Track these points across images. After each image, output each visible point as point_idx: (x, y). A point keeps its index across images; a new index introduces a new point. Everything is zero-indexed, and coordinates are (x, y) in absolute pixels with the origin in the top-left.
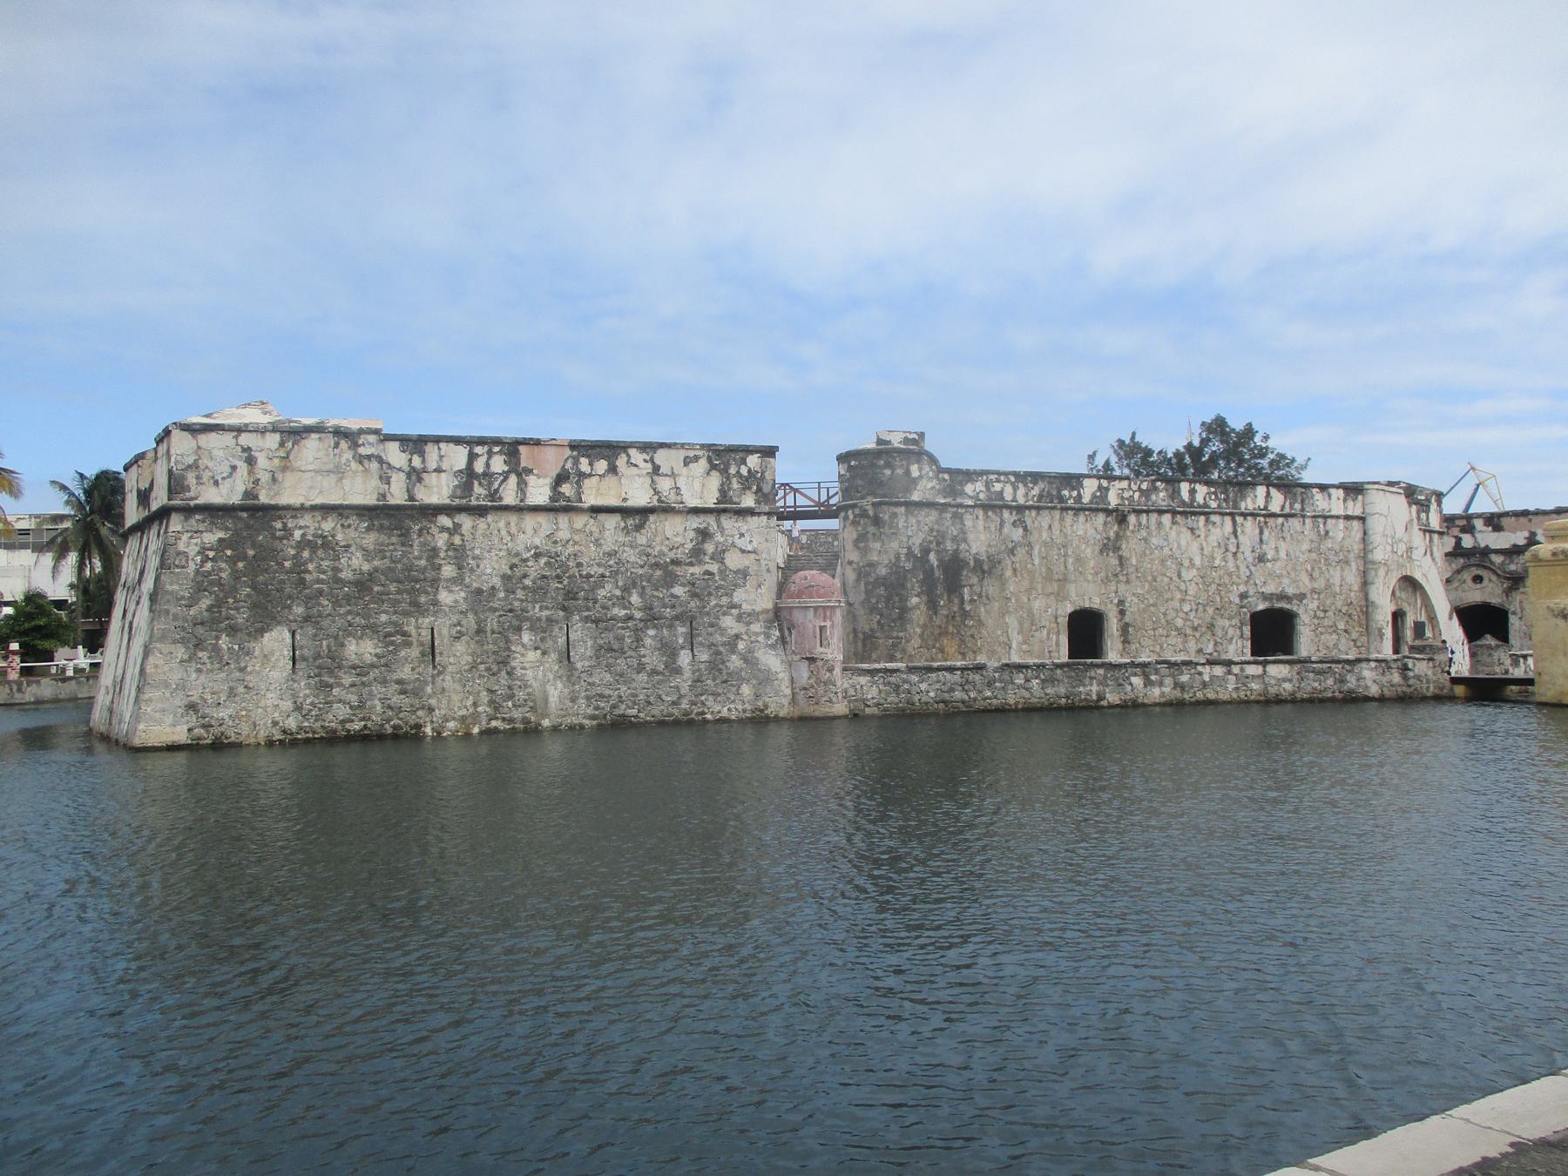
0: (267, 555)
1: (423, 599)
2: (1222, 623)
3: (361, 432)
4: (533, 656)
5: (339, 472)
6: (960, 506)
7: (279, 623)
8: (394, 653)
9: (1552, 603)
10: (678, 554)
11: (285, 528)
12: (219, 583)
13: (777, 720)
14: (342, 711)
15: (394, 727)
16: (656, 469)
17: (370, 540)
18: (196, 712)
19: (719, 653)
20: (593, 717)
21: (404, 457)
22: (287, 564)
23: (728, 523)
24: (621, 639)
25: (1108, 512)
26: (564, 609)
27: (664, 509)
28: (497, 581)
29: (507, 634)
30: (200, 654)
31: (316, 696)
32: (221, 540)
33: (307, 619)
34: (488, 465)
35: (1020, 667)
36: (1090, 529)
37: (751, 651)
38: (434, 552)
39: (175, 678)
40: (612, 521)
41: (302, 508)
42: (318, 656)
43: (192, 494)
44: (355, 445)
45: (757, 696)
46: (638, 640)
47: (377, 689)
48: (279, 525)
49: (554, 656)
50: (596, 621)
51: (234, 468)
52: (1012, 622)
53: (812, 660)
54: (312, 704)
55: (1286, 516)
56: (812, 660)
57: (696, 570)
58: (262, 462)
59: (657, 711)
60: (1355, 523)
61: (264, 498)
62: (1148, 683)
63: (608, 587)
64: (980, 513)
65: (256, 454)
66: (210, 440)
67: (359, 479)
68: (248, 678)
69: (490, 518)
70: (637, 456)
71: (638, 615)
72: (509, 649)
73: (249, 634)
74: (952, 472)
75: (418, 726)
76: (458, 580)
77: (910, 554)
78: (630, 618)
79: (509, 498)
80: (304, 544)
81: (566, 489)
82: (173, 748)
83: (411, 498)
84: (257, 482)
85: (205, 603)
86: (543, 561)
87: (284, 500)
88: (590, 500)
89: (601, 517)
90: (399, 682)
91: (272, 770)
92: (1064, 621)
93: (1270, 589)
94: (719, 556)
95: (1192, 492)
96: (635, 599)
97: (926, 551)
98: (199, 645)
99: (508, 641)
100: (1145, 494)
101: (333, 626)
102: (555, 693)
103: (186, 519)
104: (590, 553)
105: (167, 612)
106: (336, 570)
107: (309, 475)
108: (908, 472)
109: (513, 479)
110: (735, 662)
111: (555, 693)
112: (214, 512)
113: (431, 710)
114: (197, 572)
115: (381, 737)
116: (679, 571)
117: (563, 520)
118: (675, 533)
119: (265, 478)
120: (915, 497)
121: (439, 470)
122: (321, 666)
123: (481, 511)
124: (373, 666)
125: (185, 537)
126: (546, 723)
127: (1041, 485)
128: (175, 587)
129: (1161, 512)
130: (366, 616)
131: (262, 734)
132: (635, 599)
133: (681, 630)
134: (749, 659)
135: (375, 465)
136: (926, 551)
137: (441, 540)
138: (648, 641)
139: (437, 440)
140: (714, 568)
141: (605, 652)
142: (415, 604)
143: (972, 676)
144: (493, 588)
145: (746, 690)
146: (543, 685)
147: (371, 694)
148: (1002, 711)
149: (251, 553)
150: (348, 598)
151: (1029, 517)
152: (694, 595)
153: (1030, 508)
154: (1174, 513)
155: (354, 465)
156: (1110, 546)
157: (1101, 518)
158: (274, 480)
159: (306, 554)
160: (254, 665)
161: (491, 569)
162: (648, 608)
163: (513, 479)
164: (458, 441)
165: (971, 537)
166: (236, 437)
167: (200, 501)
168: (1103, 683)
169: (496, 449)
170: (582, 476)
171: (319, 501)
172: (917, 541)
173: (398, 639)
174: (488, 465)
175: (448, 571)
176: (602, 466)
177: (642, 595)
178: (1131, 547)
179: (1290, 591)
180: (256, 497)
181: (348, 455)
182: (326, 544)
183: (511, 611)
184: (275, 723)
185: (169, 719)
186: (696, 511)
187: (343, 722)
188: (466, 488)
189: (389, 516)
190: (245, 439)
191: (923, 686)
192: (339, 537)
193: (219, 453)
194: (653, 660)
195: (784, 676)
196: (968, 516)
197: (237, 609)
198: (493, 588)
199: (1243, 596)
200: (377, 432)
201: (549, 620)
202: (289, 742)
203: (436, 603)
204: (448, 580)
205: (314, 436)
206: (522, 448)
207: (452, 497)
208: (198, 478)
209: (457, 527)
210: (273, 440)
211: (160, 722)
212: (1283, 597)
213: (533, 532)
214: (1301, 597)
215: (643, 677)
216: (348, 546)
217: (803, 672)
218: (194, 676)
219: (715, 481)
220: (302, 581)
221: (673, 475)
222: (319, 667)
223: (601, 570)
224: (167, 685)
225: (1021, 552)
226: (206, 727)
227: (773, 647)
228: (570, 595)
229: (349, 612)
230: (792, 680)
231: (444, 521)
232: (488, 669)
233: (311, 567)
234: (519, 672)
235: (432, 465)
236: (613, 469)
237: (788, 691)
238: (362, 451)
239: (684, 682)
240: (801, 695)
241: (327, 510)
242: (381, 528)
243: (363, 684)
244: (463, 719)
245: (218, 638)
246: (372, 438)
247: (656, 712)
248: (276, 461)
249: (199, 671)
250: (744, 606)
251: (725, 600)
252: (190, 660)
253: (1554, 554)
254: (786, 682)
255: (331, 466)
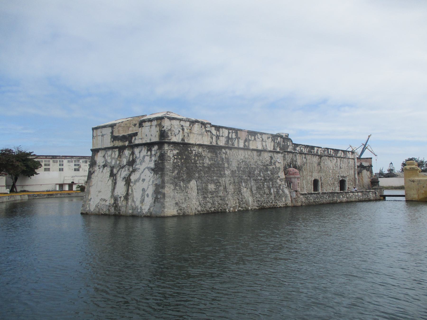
0: (188, 158)
1: (222, 173)
2: (335, 183)
3: (207, 123)
4: (245, 189)
5: (202, 134)
6: (296, 153)
7: (193, 179)
8: (218, 188)
9: (409, 179)
10: (268, 163)
11: (191, 150)
12: (178, 166)
13: (289, 207)
14: (209, 205)
15: (221, 210)
16: (263, 139)
17: (209, 155)
18: (178, 205)
19: (277, 189)
20: (258, 207)
21: (215, 131)
22: (193, 161)
23: (275, 155)
24: (260, 185)
25: (318, 155)
26: (249, 176)
27: (264, 150)
28: (236, 168)
29: (240, 183)
30: (177, 187)
31: (204, 201)
32: (177, 153)
33: (199, 178)
34: (232, 136)
35: (325, 193)
36: (315, 159)
37: (283, 189)
38: (223, 159)
39: (172, 195)
40: (255, 153)
41: (196, 145)
42: (203, 189)
43: (170, 138)
44: (205, 127)
45: (285, 201)
46: (264, 186)
47: (216, 198)
48: (190, 150)
49: (249, 189)
50: (255, 180)
51: (179, 131)
52: (304, 182)
53: (296, 191)
54: (203, 203)
55: (344, 158)
56: (296, 191)
57: (271, 167)
58: (186, 130)
59: (269, 204)
60: (353, 160)
61: (186, 141)
62: (343, 197)
63: (257, 171)
64: (299, 154)
65: (184, 128)
66: (175, 122)
67: (206, 137)
68: (188, 195)
69: (233, 150)
70: (259, 136)
71: (263, 179)
72: (240, 187)
73: (187, 182)
74: (295, 144)
75: (225, 209)
76: (228, 168)
77: (288, 164)
78: (261, 179)
79: (236, 146)
80: (196, 155)
81: (246, 144)
82: (174, 216)
83: (217, 144)
84: (184, 136)
85: (176, 172)
86: (244, 163)
87: (191, 142)
88: (251, 147)
89: (253, 152)
90: (220, 196)
91: (195, 223)
92: (312, 182)
93: (342, 175)
94: (275, 164)
95: (331, 151)
96: (262, 174)
97: (290, 164)
98: (176, 185)
99: (240, 185)
100: (324, 151)
101: (205, 180)
102: (250, 199)
103: (169, 146)
104: (252, 161)
105: (168, 174)
106: (203, 163)
107: (196, 135)
108: (287, 144)
109: (237, 140)
110: (281, 192)
111: (250, 199)
112: (174, 143)
113: (227, 205)
114: (173, 162)
115: (218, 212)
116: (269, 167)
117: (246, 152)
118: (266, 156)
119: (186, 135)
120: (289, 150)
121: (222, 136)
122: (203, 191)
123: (230, 148)
124: (214, 192)
125: (169, 151)
126: (250, 208)
127: (309, 148)
128: (169, 167)
129: (326, 156)
130: (211, 178)
131: (193, 212)
132: (262, 174)
133: (271, 183)
134: (283, 192)
135: (209, 134)
136: (290, 164)
137: (224, 156)
138: (265, 186)
139: (222, 127)
140: (274, 167)
141: (258, 188)
142: (221, 174)
143: (318, 196)
144: (235, 170)
145: (283, 199)
146: (248, 198)
147: (215, 200)
148: (323, 204)
149: (185, 157)
150: (207, 172)
151: (307, 155)
152: (272, 174)
153: (307, 154)
154: (328, 156)
155: (205, 133)
156: (319, 164)
157: (317, 157)
158: (188, 136)
159: (196, 158)
160: (189, 191)
161: (234, 165)
162: (264, 177)
163: (237, 140)
164: (226, 128)
165: (298, 160)
166: (180, 122)
167: (171, 141)
168: (337, 197)
169: (234, 131)
170: (250, 140)
171: (198, 143)
172: (289, 161)
173: (218, 184)
174: (232, 136)
175: (226, 165)
176: (253, 138)
177: (263, 173)
178: (322, 164)
179: (345, 176)
180: (184, 141)
181: (204, 130)
182: (199, 155)
183: (239, 177)
184: (196, 209)
185: (172, 208)
186: (270, 151)
187: (210, 208)
188: (227, 142)
189: (213, 148)
190: (182, 123)
191: (311, 198)
192: (203, 154)
193: (176, 126)
194: (267, 191)
195: (289, 195)
196: (297, 156)
197: (183, 174)
198: (235, 170)
199: (338, 177)
200: (210, 124)
201: (247, 179)
202: (199, 215)
203: (225, 174)
204: (226, 168)
205: (197, 124)
206: (238, 132)
207: (225, 144)
208: (171, 133)
209: (226, 152)
210: (188, 124)
211: (170, 209)
212: (344, 177)
213: (242, 155)
214: (346, 177)
215: (265, 195)
216: (205, 157)
217: (294, 195)
218: (176, 194)
219: (272, 144)
220: (196, 166)
221: (265, 142)
222: (203, 192)
223: (255, 166)
224: (171, 197)
225: (305, 164)
226: (180, 210)
227: (286, 188)
228: (250, 173)
229: (208, 176)
230: (291, 196)
231: (223, 151)
232: (237, 193)
233: (198, 162)
234: (243, 194)
235: (221, 135)
236: (255, 139)
237: (290, 199)
238: (207, 129)
239: (272, 197)
240: (294, 201)
241: (200, 145)
242: (211, 152)
243: (213, 197)
244: (234, 207)
245: (180, 183)
246: (209, 126)
247: (269, 205)
248: (189, 130)
249: (177, 193)
250: (281, 177)
251: (277, 175)
252: (175, 189)
253: (410, 168)
254: (290, 197)
255: (200, 133)
